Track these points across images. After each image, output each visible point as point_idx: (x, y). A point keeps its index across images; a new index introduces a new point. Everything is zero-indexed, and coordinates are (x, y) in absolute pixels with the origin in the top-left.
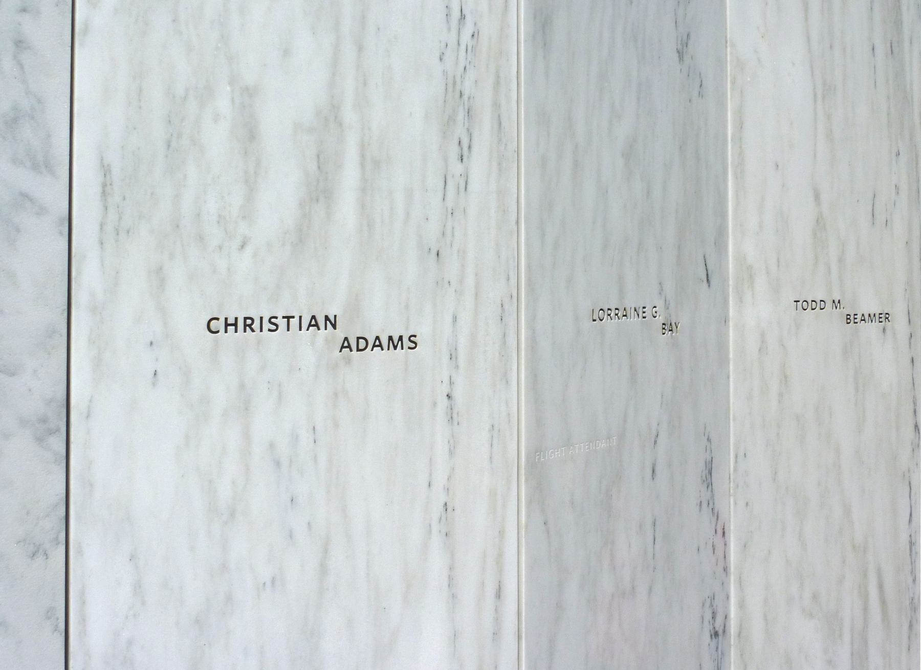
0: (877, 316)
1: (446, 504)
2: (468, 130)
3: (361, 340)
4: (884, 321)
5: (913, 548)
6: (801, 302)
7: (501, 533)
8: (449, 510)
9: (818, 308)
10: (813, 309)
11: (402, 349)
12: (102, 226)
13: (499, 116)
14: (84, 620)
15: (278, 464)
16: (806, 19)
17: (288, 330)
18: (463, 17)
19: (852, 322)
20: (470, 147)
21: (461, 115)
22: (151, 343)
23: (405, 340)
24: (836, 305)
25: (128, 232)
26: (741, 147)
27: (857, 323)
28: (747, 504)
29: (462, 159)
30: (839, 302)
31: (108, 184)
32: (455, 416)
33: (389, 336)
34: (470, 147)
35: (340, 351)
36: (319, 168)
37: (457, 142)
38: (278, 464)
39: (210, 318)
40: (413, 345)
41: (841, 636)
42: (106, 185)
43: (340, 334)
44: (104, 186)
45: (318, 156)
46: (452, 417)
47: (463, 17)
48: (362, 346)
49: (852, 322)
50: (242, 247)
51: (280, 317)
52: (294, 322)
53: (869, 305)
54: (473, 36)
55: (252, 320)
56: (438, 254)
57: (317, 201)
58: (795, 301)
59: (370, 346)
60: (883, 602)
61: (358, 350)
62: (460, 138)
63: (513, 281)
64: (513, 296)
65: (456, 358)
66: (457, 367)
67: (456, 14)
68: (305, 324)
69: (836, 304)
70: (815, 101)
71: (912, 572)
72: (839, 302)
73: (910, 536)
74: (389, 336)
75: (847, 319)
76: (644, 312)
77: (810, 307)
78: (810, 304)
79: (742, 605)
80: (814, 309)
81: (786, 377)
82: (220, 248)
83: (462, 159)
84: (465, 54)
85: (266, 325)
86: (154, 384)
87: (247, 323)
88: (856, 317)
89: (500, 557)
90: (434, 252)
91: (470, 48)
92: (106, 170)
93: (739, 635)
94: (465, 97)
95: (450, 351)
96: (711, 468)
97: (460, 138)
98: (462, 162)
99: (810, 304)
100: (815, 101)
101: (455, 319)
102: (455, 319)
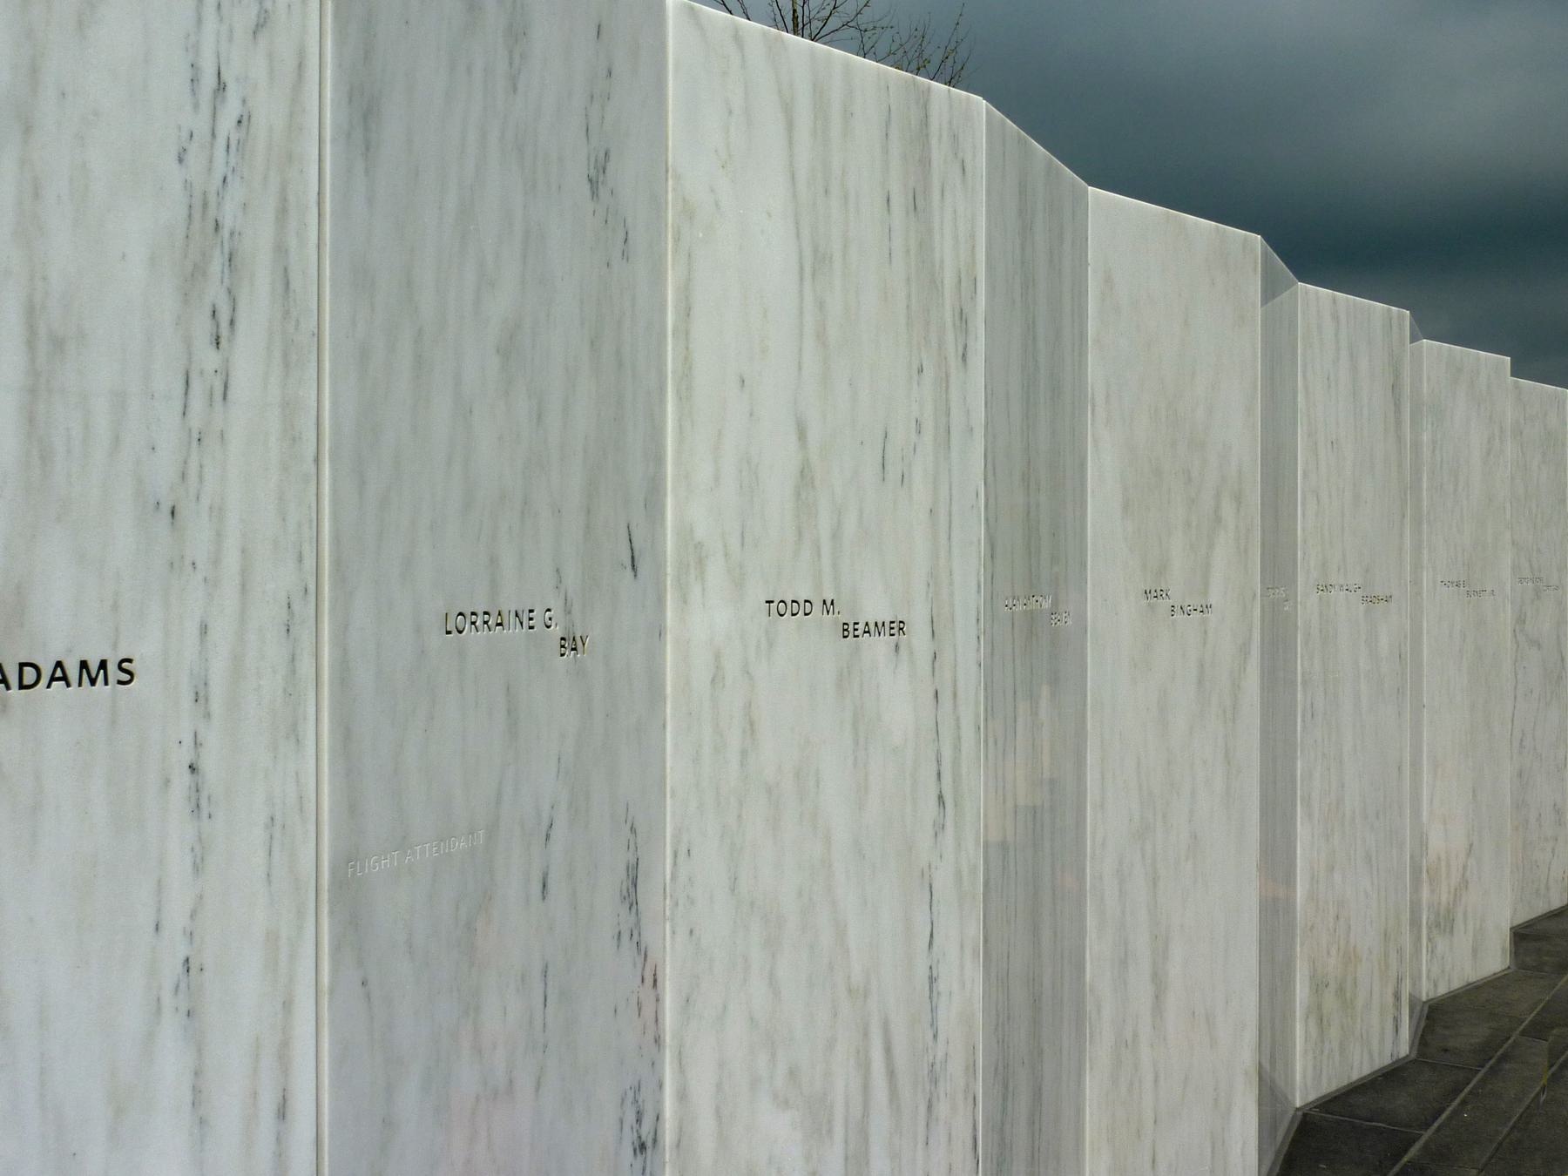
0: (887, 625)
6: (776, 604)
7: (288, 1005)
9: (801, 612)
11: (106, 683)
13: (286, 270)
18: (221, 87)
19: (851, 635)
20: (232, 322)
21: (217, 265)
23: (112, 668)
24: (94, 675)
27: (858, 636)
28: (691, 932)
29: (218, 344)
30: (832, 603)
32: (204, 803)
34: (232, 322)
37: (208, 313)
41: (830, 1131)
49: (851, 635)
53: (875, 609)
54: (239, 122)
58: (767, 602)
60: (891, 1074)
65: (207, 700)
66: (208, 715)
67: (208, 81)
69: (829, 606)
70: (802, 279)
71: (932, 1025)
72: (832, 603)
73: (931, 968)
75: (844, 630)
76: (531, 619)
77: (789, 611)
79: (682, 1096)
80: (796, 614)
81: (752, 724)
83: (218, 344)
88: (856, 626)
90: (166, 509)
94: (225, 233)
100: (802, 279)
101: (204, 630)
102: (204, 630)
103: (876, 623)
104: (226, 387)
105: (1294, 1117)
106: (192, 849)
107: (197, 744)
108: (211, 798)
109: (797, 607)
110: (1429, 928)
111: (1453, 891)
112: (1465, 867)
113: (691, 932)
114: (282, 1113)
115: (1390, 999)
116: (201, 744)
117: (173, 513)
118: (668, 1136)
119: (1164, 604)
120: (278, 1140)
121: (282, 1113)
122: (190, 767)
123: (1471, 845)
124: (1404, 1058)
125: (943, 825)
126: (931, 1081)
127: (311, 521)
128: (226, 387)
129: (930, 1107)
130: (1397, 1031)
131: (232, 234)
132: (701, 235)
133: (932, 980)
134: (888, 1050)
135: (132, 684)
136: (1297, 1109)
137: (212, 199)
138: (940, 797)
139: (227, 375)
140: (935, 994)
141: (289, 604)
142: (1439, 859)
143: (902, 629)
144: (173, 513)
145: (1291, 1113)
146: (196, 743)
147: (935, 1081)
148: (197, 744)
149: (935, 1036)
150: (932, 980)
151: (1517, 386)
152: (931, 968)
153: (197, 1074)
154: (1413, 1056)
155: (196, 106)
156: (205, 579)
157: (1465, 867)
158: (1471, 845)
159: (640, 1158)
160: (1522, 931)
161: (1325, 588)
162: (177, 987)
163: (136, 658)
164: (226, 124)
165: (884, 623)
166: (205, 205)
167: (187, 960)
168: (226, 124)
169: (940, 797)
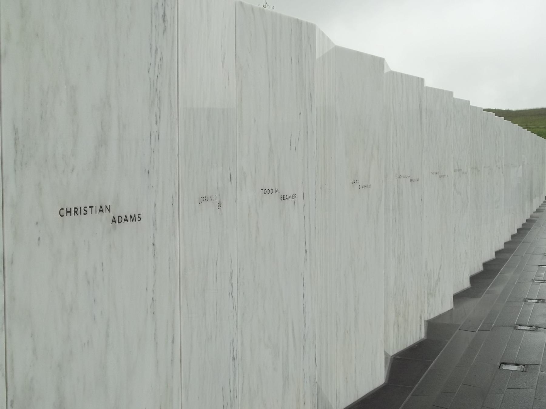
0: (292, 195)
2: (159, 108)
4: (294, 199)
5: (305, 310)
6: (264, 190)
9: (270, 193)
10: (268, 193)
12: (15, 161)
13: (171, 101)
14: (13, 370)
15: (89, 282)
17: (71, 215)
18: (157, 50)
20: (160, 117)
21: (156, 100)
22: (37, 223)
23: (137, 217)
25: (26, 164)
26: (241, 111)
28: (244, 293)
31: (446, 176)
32: (156, 254)
34: (160, 117)
35: (112, 223)
36: (102, 129)
38: (89, 282)
40: (85, 212)
42: (16, 139)
43: (111, 215)
44: (15, 139)
45: (102, 123)
47: (157, 50)
48: (120, 221)
50: (73, 171)
52: (94, 209)
53: (288, 192)
55: (77, 209)
56: (148, 173)
57: (102, 146)
58: (262, 190)
59: (123, 221)
60: (294, 337)
61: (119, 223)
62: (156, 113)
63: (177, 185)
65: (156, 225)
66: (156, 229)
68: (98, 211)
69: (277, 190)
71: (304, 322)
73: (304, 304)
77: (267, 193)
78: (270, 191)
79: (242, 344)
82: (64, 171)
85: (83, 212)
86: (39, 244)
91: (159, 66)
92: (16, 131)
93: (241, 359)
94: (158, 91)
95: (154, 221)
97: (156, 113)
99: (267, 191)
101: (155, 205)
102: (155, 205)
103: (131, 215)
105: (391, 358)
109: (267, 191)
110: (428, 295)
111: (435, 282)
112: (439, 273)
113: (244, 293)
114: (173, 342)
115: (419, 319)
118: (240, 357)
119: (357, 186)
120: (172, 349)
121: (173, 342)
123: (441, 266)
124: (423, 339)
125: (307, 259)
126: (304, 340)
127: (177, 173)
129: (304, 348)
130: (421, 329)
131: (159, 92)
132: (244, 75)
133: (304, 308)
134: (293, 330)
135: (141, 221)
136: (392, 356)
137: (155, 82)
138: (306, 250)
139: (159, 132)
140: (305, 313)
142: (431, 270)
143: (295, 197)
145: (390, 357)
147: (305, 340)
149: (305, 326)
150: (304, 308)
151: (519, 128)
152: (304, 304)
153: (155, 330)
154: (426, 338)
155: (151, 56)
156: (155, 191)
157: (439, 273)
158: (441, 266)
159: (234, 362)
160: (398, 357)
161: (399, 177)
163: (141, 214)
164: (158, 60)
166: (154, 84)
167: (153, 298)
168: (158, 60)
169: (306, 250)
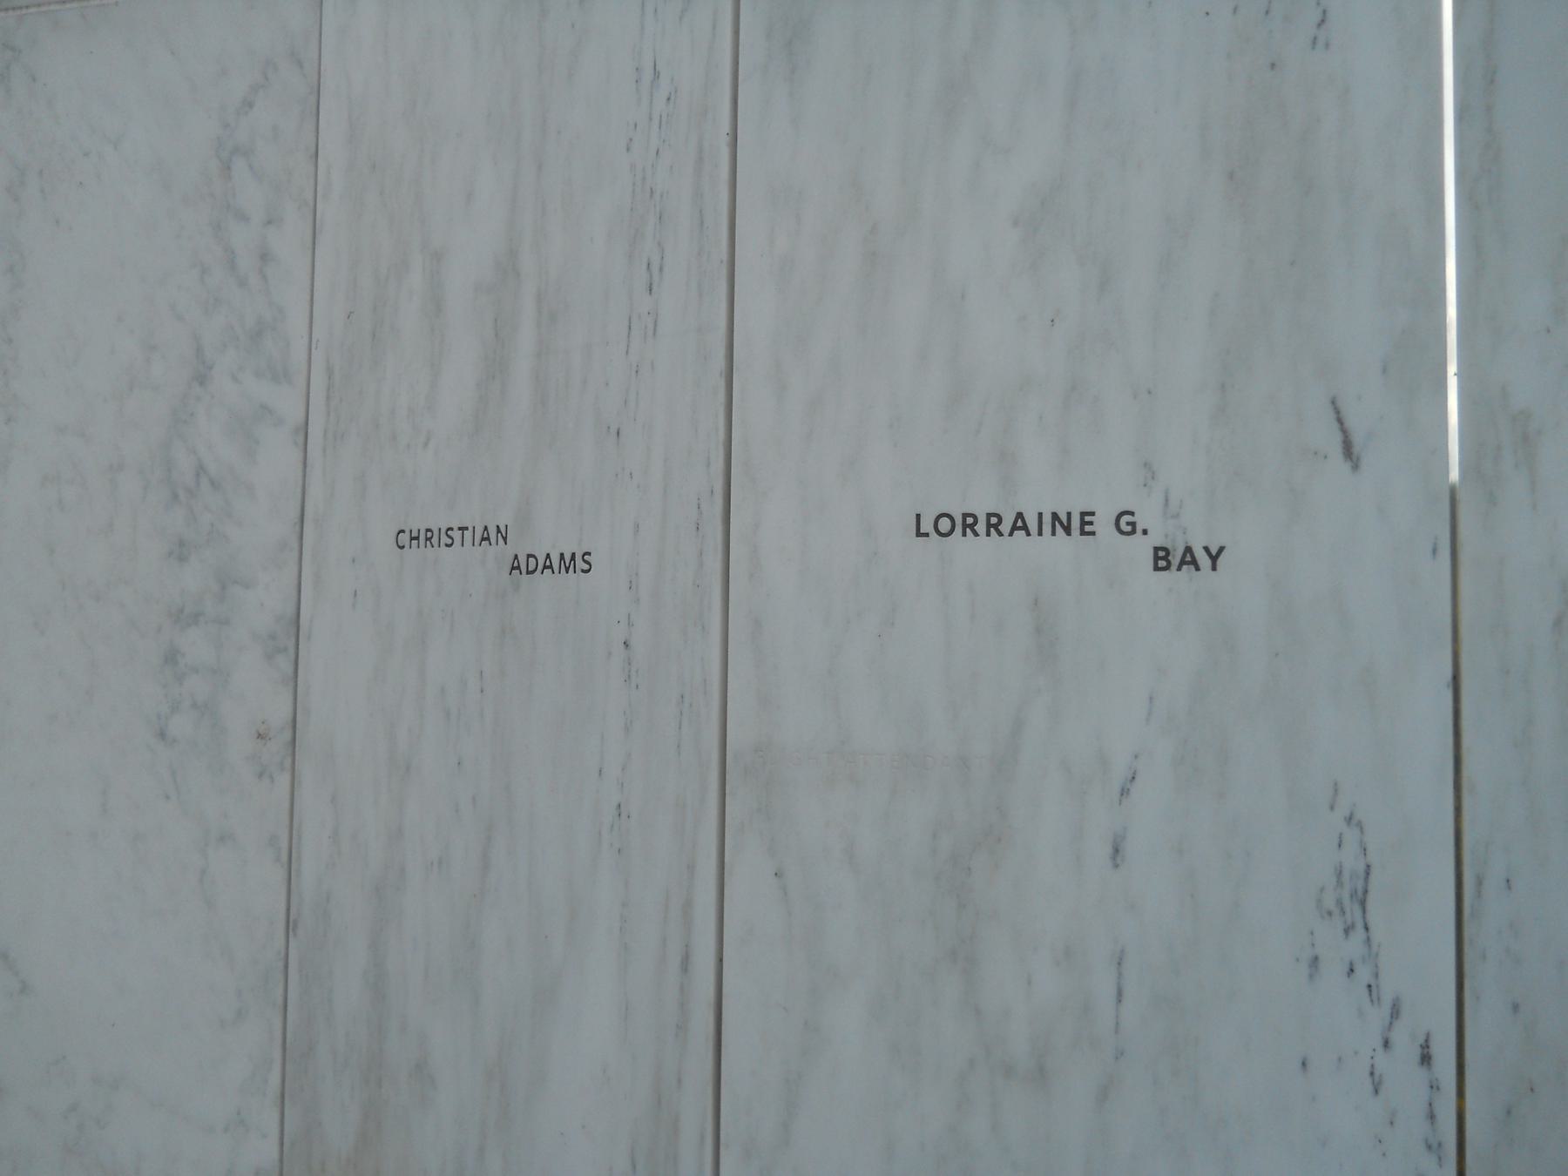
1: (619, 805)
2: (659, 244)
3: (530, 559)
7: (691, 868)
8: (624, 816)
16: (1370, 995)
20: (661, 269)
29: (650, 290)
33: (1070, 535)
34: (661, 269)
37: (644, 266)
39: (1114, 527)
43: (509, 551)
46: (629, 676)
51: (456, 528)
53: (550, 540)
54: (669, 99)
58: (1221, 549)
59: (540, 567)
61: (528, 572)
64: (714, 491)
66: (638, 601)
67: (648, 75)
74: (1070, 535)
83: (650, 290)
84: (658, 130)
87: (428, 536)
89: (687, 907)
90: (613, 430)
91: (664, 119)
96: (1366, 892)
98: (650, 293)
101: (637, 527)
102: (637, 527)
103: (562, 555)
104: (655, 325)
106: (625, 712)
107: (630, 624)
108: (483, 674)
116: (633, 625)
117: (618, 433)
122: (625, 643)
128: (655, 325)
141: (699, 505)
144: (618, 433)
146: (629, 624)
148: (630, 624)
162: (612, 826)
165: (573, 554)
